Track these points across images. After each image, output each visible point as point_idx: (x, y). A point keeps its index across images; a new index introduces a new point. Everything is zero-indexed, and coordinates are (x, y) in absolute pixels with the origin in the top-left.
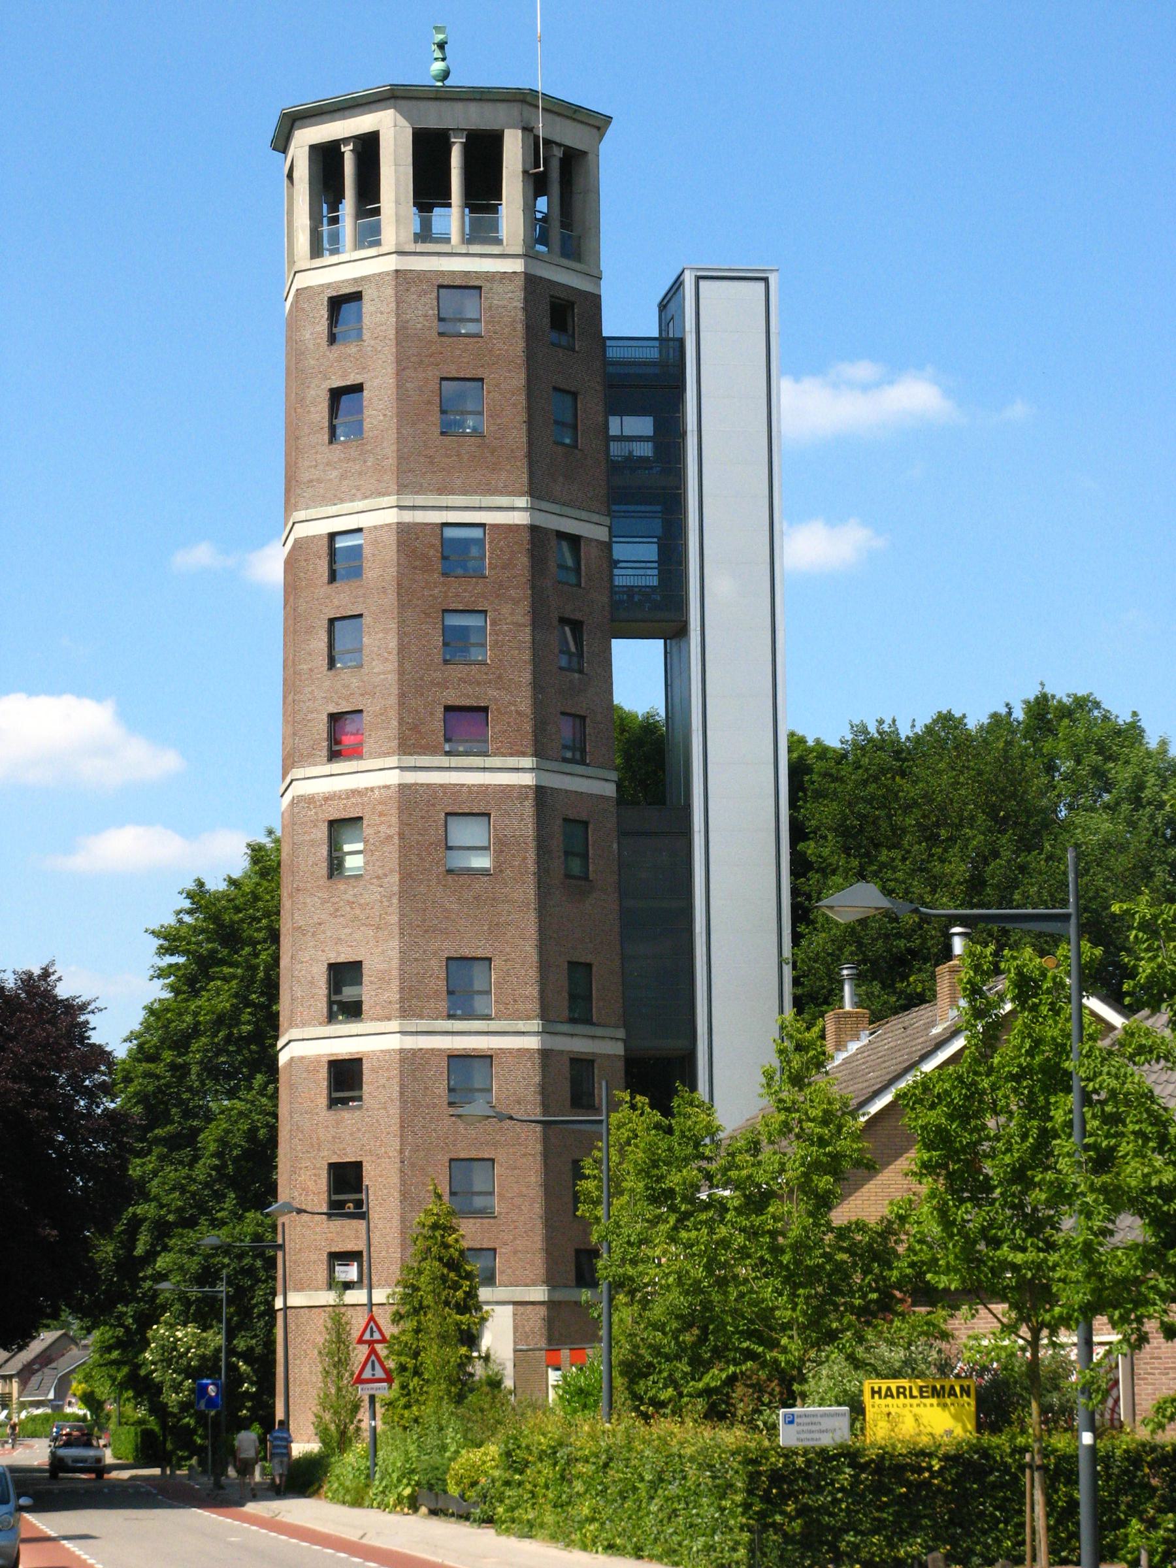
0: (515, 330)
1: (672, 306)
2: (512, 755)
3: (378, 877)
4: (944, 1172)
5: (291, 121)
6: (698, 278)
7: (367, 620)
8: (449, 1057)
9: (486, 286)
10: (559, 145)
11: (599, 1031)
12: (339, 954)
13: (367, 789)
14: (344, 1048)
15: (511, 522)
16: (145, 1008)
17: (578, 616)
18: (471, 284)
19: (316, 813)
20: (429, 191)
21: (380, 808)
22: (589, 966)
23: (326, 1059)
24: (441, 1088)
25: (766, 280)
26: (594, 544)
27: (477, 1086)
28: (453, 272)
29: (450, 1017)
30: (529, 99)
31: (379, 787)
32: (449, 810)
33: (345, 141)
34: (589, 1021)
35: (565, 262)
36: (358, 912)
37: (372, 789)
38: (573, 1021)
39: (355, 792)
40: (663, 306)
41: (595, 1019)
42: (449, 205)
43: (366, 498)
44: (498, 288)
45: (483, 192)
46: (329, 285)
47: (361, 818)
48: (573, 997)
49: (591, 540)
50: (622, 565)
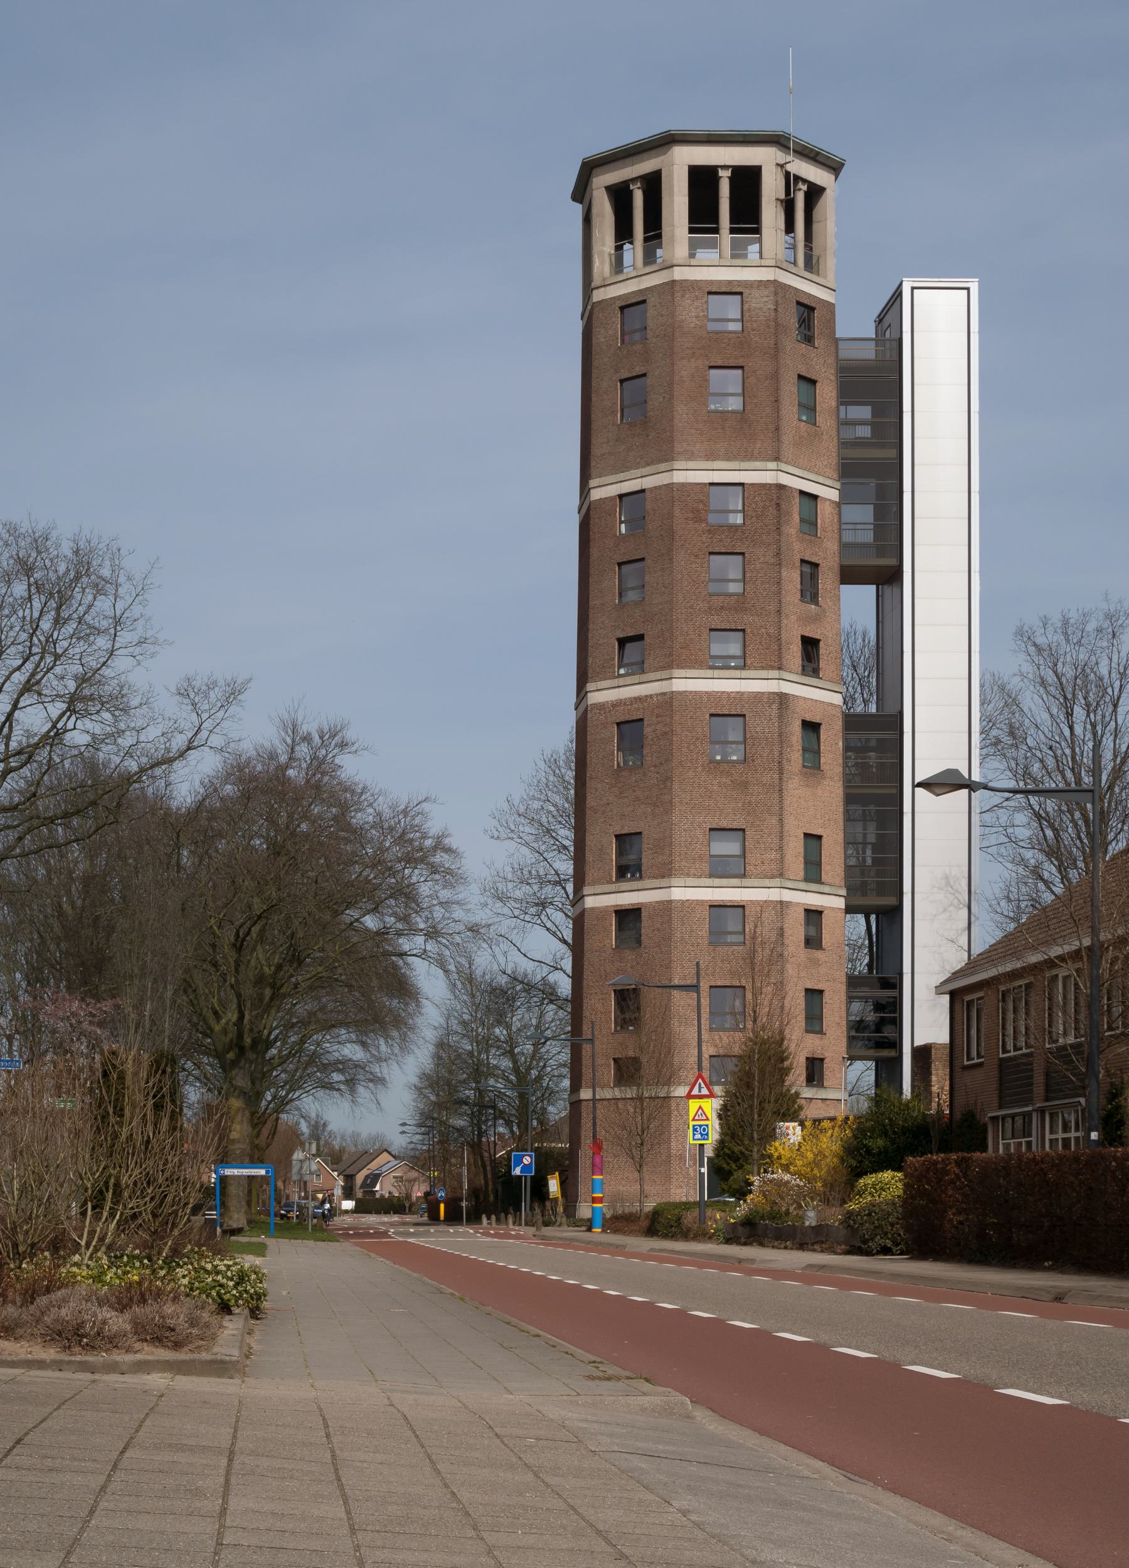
0: (768, 327)
1: (887, 320)
2: (763, 668)
3: (655, 766)
4: (536, 887)
5: (589, 168)
6: (913, 288)
7: (648, 562)
8: (711, 906)
9: (746, 292)
10: (805, 181)
11: (827, 889)
12: (623, 827)
13: (474, 1218)
14: (627, 899)
15: (764, 482)
16: (939, 990)
17: (814, 559)
18: (734, 290)
19: (606, 718)
20: (702, 215)
21: (656, 711)
22: (819, 837)
23: (612, 909)
24: (704, 931)
25: (968, 289)
26: (827, 503)
27: (730, 929)
28: (720, 281)
29: (711, 876)
30: (782, 141)
31: (657, 695)
32: (713, 711)
33: (633, 180)
34: (819, 881)
35: (807, 275)
36: (639, 793)
37: (651, 696)
38: (807, 880)
39: (638, 699)
40: (880, 320)
41: (824, 878)
42: (716, 231)
43: (648, 465)
44: (756, 293)
45: (747, 216)
46: (619, 298)
47: (642, 720)
48: (807, 862)
49: (826, 499)
50: (384, 1169)
